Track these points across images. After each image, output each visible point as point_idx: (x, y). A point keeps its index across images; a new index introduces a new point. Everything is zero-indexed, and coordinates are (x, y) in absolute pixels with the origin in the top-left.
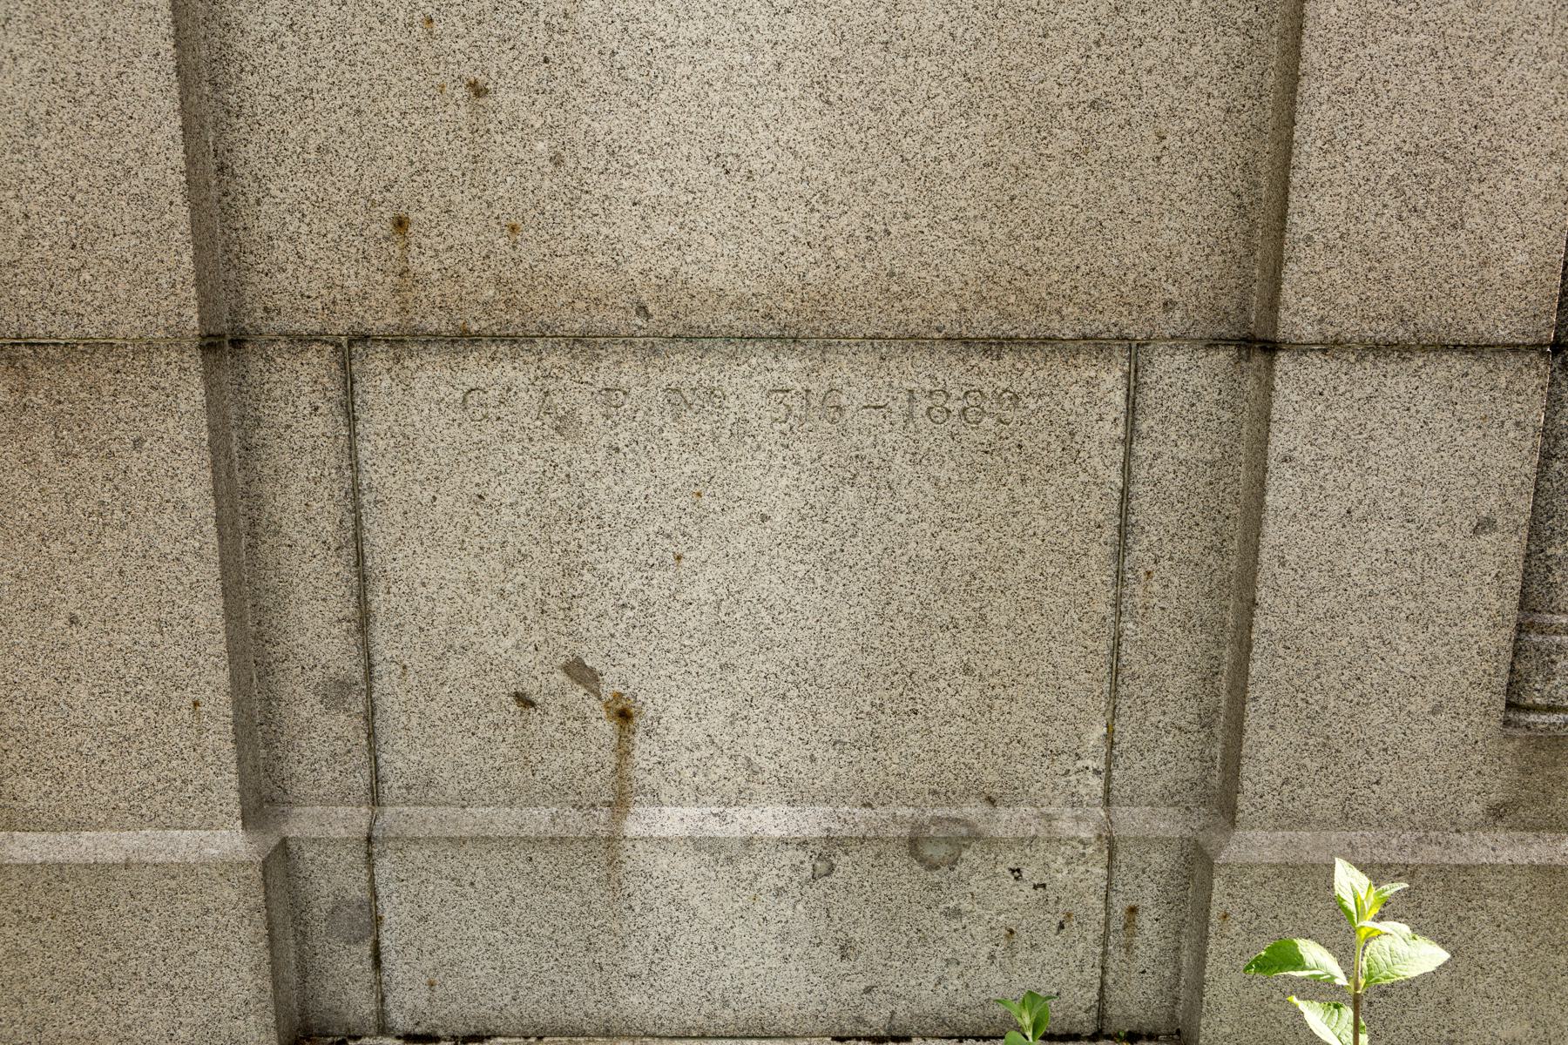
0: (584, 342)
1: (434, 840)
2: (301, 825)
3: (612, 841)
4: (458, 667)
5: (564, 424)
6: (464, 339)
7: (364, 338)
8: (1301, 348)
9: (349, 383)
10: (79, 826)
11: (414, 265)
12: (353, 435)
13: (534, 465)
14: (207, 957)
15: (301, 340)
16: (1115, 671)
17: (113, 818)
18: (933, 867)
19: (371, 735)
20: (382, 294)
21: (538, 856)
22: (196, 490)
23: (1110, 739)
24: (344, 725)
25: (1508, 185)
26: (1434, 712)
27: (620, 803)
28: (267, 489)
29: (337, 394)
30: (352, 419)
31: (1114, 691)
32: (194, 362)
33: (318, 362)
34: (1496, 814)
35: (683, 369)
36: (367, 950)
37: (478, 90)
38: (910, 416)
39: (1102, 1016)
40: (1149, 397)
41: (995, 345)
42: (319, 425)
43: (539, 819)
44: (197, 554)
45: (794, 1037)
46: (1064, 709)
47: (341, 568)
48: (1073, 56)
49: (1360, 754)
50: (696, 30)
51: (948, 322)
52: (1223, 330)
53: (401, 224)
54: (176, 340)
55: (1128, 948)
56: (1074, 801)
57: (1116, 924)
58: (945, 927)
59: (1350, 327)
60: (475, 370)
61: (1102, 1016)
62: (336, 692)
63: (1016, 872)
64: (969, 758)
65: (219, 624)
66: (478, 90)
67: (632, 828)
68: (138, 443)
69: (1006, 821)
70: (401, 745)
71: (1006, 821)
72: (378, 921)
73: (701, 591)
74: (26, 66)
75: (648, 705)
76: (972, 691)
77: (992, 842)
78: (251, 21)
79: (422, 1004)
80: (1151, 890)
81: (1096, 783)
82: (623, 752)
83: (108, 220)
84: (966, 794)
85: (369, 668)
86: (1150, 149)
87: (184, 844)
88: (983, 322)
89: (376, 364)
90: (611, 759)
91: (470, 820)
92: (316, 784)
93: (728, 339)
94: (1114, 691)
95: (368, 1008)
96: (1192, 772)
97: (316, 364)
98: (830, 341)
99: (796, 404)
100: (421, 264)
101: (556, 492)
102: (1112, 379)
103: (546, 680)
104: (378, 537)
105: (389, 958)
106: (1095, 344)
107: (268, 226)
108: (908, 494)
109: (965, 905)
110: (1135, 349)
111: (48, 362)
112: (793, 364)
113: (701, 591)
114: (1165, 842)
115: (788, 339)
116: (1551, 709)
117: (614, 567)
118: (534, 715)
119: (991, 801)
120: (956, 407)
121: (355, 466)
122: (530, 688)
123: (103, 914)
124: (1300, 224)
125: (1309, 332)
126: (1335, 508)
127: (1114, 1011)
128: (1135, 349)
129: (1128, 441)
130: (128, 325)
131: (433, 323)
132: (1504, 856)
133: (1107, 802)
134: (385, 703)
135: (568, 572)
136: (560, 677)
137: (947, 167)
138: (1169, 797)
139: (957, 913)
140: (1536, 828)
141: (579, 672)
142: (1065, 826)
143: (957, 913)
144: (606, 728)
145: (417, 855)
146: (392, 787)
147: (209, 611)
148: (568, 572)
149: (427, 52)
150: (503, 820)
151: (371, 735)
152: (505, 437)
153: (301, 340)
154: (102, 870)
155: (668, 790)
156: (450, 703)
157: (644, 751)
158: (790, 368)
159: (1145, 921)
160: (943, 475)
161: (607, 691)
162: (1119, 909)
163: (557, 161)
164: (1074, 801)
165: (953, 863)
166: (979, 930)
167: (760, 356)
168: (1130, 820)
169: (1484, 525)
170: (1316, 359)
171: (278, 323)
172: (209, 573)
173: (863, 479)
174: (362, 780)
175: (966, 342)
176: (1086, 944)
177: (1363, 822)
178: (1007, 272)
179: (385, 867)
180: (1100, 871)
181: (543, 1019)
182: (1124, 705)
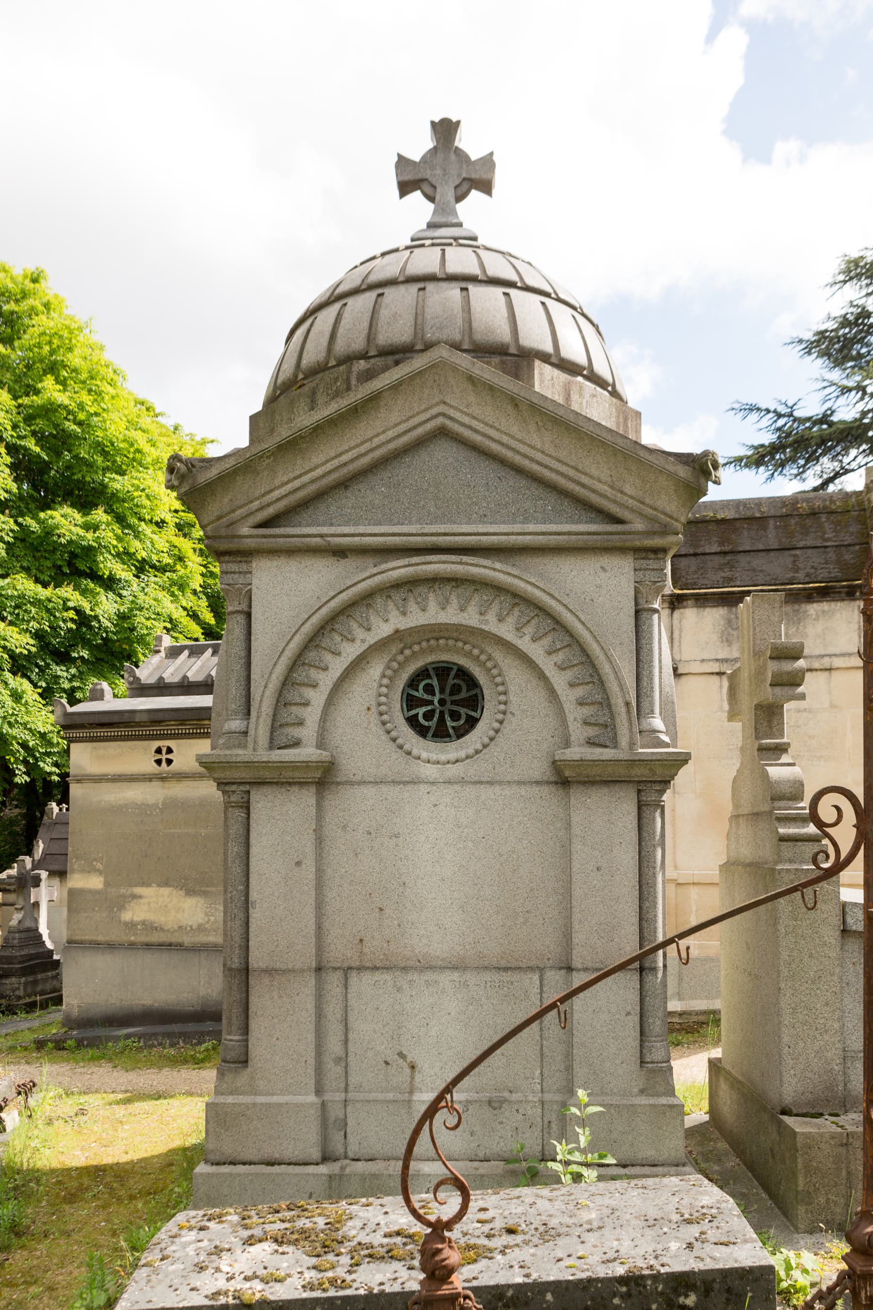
0: (405, 969)
1: (362, 1101)
2: (327, 1097)
3: (409, 1101)
4: (370, 1054)
5: (399, 990)
6: (375, 968)
7: (351, 968)
8: (578, 970)
9: (346, 980)
10: (273, 1094)
11: (364, 950)
12: (347, 992)
13: (391, 1000)
14: (305, 1130)
15: (335, 969)
16: (542, 1055)
17: (282, 1093)
18: (495, 1109)
19: (346, 1073)
20: (356, 957)
21: (390, 1105)
22: (310, 1005)
23: (541, 1074)
24: (339, 1070)
25: (623, 931)
26: (622, 1063)
27: (411, 1092)
28: (324, 1006)
29: (343, 982)
30: (346, 988)
31: (542, 1060)
32: (313, 975)
33: (339, 974)
34: (642, 1091)
35: (429, 976)
36: (343, 1133)
37: (381, 910)
38: (486, 987)
39: (543, 1154)
40: (545, 982)
41: (506, 969)
42: (339, 990)
43: (390, 1096)
44: (310, 1022)
45: (318, 668)
46: (529, 1065)
47: (341, 1027)
48: (522, 901)
49: (604, 1075)
50: (433, 895)
51: (494, 962)
52: (563, 965)
53: (361, 941)
54: (309, 969)
55: (549, 1133)
56: (533, 1092)
57: (545, 1126)
58: (499, 1127)
59: (590, 965)
60: (378, 976)
61: (543, 1154)
62: (338, 1060)
63: (517, 1110)
64: (504, 1079)
65: (314, 1040)
66: (381, 910)
67: (415, 1098)
68: (298, 994)
69: (514, 1097)
70: (354, 1075)
71: (514, 1097)
72: (346, 1124)
73: (433, 1033)
74: (282, 907)
75: (419, 1064)
76: (504, 1060)
77: (510, 1102)
78: (329, 894)
79: (357, 1149)
80: (554, 1116)
81: (539, 1087)
82: (412, 1078)
83: (296, 941)
84: (504, 1090)
85: (347, 1054)
86: (542, 922)
87: (300, 1099)
88: (503, 963)
89: (353, 974)
90: (409, 1079)
91: (372, 1096)
92: (331, 1086)
93: (440, 968)
94: (542, 1060)
95: (342, 1151)
96: (564, 1083)
97: (339, 974)
98: (465, 969)
99: (457, 984)
100: (366, 950)
101: (397, 1007)
102: (536, 977)
103: (393, 1058)
104: (351, 1019)
105: (349, 1135)
106: (531, 969)
107: (329, 941)
108: (486, 1007)
109: (504, 1120)
110: (541, 970)
111: (279, 974)
112: (456, 974)
113: (433, 1033)
114: (557, 1102)
115: (455, 968)
116: (652, 1062)
117: (411, 1027)
118: (389, 1067)
119: (511, 1092)
120: (497, 985)
121: (347, 1000)
122: (388, 1059)
123: (279, 1117)
124: (575, 941)
125: (580, 966)
126: (591, 1010)
127: (546, 1153)
128: (541, 970)
129: (541, 993)
130: (298, 966)
131: (368, 965)
132: (643, 1102)
133: (542, 1092)
134: (350, 1063)
135: (399, 1028)
136: (396, 1056)
137: (493, 926)
138: (559, 1091)
139: (502, 1123)
140: (653, 1096)
141: (401, 1055)
142: (530, 1098)
143: (502, 1123)
144: (408, 1071)
145: (358, 1105)
146: (351, 1088)
147: (311, 1037)
148: (399, 1028)
149: (370, 901)
150: (380, 1096)
151: (346, 1073)
152: (385, 993)
153: (335, 969)
154: (280, 1105)
155: (424, 1088)
156: (367, 1064)
157: (418, 1078)
158: (455, 975)
159: (553, 1125)
160: (494, 1002)
161: (408, 1061)
162: (546, 1122)
163: (399, 926)
164: (533, 1092)
165: (500, 1108)
166: (508, 1128)
167: (448, 973)
168: (548, 1097)
169: (628, 1014)
170: (582, 973)
171: (330, 964)
172: (312, 1027)
173: (474, 1003)
174: (343, 1085)
175: (499, 969)
176: (537, 1133)
177: (607, 1094)
178: (508, 952)
179: (349, 1109)
180: (540, 1110)
181: (390, 1155)
182: (545, 1065)
